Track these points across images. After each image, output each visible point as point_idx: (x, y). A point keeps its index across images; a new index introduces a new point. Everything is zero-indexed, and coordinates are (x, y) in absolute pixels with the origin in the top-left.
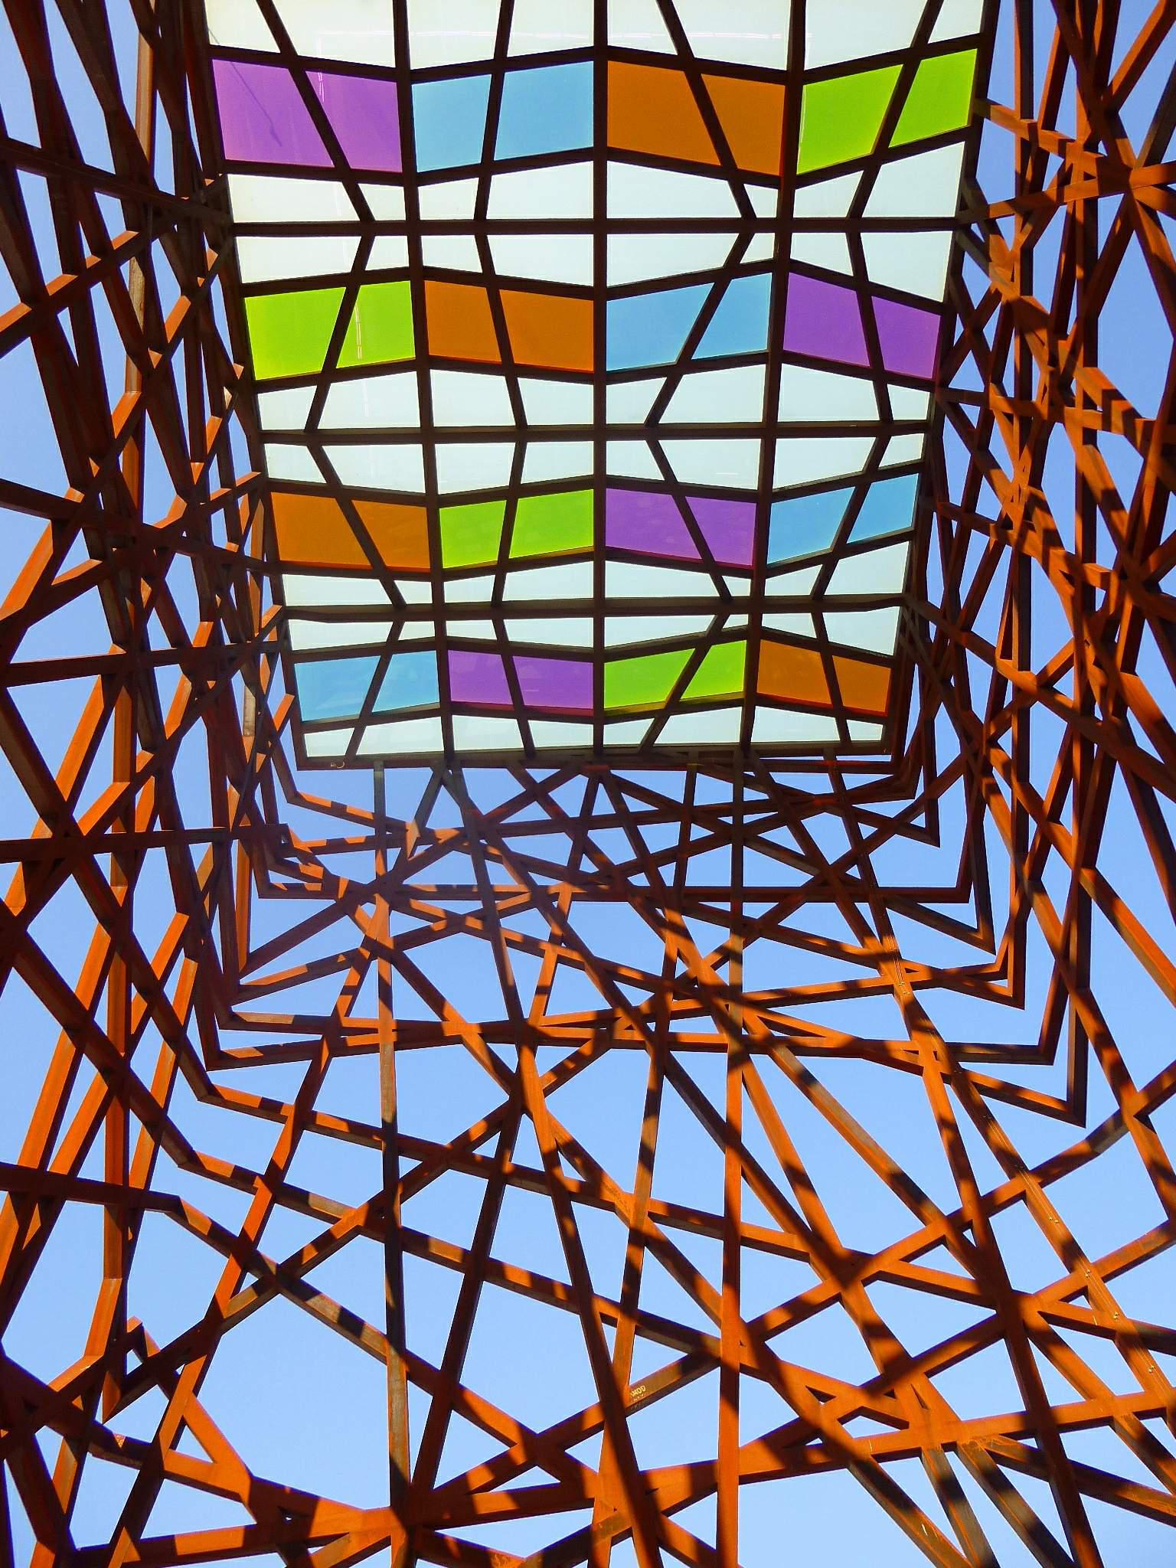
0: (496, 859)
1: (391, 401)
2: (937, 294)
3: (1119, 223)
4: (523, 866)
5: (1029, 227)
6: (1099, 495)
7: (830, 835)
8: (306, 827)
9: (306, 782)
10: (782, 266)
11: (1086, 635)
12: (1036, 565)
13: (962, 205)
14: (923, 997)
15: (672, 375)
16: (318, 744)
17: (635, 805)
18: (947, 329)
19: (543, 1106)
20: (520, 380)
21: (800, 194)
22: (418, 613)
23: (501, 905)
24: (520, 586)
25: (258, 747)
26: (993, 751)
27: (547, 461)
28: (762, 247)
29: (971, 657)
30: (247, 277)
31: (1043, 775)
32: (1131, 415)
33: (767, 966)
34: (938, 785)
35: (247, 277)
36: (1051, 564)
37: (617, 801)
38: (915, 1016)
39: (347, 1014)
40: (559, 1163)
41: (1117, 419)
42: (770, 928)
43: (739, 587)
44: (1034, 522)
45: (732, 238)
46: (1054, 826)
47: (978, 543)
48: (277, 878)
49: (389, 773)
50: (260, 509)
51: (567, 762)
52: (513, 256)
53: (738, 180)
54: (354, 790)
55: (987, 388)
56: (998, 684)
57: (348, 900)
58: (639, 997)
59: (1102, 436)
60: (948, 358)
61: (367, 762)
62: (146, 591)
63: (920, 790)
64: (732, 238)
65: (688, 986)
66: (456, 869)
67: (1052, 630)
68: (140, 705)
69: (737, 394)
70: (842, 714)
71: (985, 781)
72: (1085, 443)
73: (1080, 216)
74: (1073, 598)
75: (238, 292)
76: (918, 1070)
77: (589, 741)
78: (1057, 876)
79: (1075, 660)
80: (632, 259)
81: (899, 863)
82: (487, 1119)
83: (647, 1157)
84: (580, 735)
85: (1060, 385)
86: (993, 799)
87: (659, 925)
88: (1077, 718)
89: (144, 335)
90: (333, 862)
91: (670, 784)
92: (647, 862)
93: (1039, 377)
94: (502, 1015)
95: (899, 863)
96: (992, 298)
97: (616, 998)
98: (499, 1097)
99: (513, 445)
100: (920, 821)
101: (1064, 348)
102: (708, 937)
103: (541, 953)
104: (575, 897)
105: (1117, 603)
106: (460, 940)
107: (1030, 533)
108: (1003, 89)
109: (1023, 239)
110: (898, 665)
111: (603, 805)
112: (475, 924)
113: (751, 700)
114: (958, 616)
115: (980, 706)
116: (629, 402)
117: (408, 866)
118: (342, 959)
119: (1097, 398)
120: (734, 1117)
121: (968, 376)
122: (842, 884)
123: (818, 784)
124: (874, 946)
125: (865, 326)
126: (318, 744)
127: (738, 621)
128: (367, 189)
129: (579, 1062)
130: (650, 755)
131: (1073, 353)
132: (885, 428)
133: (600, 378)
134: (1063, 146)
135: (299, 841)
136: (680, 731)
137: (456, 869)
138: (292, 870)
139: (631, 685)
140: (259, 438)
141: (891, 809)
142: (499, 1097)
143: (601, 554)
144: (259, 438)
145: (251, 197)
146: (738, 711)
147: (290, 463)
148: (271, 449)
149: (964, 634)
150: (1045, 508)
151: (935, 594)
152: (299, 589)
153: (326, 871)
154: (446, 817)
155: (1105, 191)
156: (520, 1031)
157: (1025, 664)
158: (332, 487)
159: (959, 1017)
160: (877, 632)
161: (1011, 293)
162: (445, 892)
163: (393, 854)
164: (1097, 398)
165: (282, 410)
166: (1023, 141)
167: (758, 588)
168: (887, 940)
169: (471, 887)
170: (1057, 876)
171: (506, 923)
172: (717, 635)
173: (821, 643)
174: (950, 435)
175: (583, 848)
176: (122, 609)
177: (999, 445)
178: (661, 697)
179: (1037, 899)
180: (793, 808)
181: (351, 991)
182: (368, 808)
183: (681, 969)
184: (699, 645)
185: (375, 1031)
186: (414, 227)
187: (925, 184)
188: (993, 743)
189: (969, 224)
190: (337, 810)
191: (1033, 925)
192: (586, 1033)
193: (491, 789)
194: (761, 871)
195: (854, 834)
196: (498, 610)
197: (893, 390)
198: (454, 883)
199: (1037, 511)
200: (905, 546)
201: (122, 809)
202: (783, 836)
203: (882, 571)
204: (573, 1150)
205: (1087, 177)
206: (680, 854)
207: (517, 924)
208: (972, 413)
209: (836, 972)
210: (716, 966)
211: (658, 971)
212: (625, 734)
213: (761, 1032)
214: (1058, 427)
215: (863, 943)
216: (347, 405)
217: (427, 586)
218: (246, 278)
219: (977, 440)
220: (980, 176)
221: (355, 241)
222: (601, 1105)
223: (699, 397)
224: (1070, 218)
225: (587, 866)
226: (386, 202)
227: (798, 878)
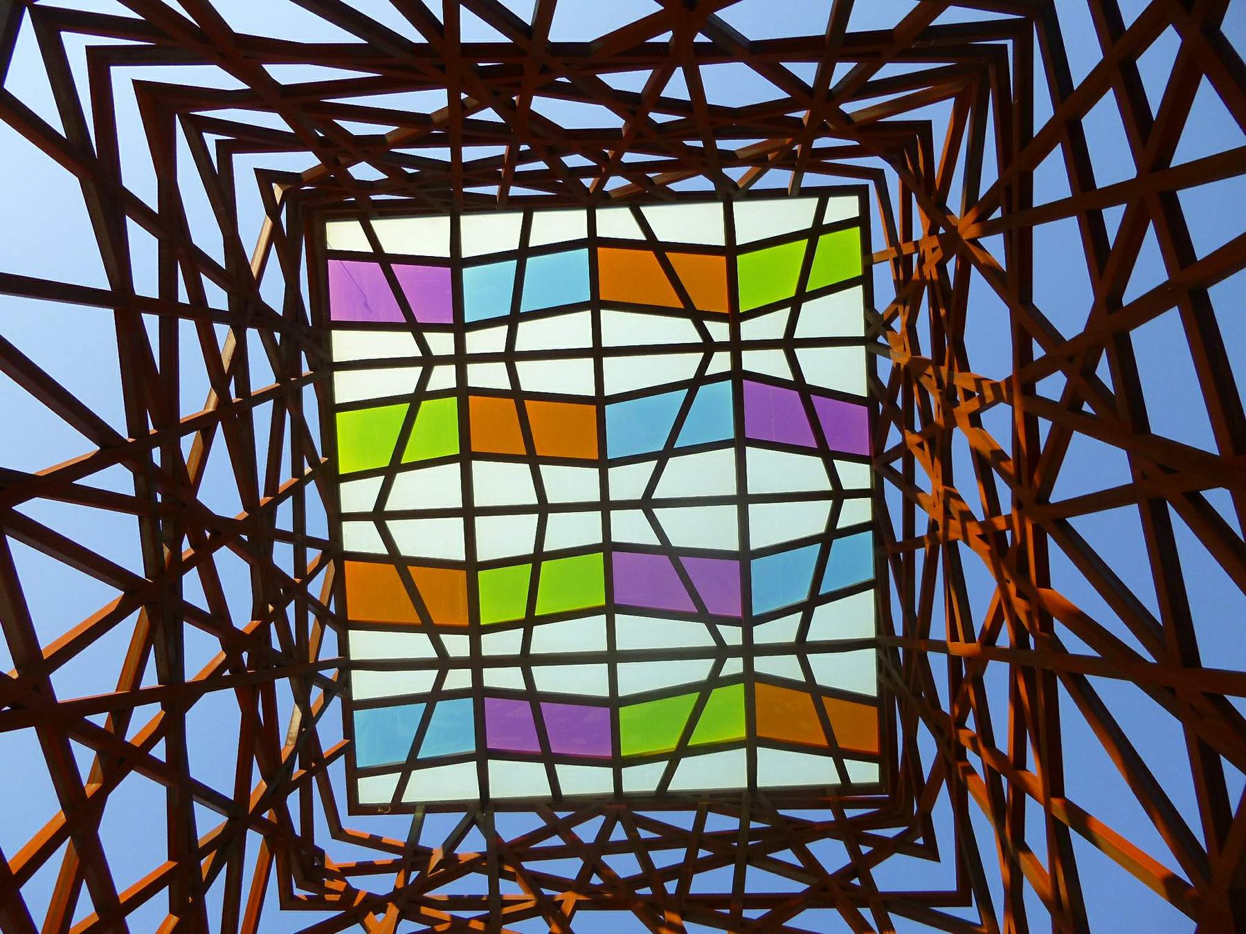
0: (511, 877)
1: (441, 486)
4: (535, 881)
5: (908, 308)
6: (989, 456)
7: (832, 855)
8: (338, 854)
10: (737, 375)
11: (1006, 575)
15: (661, 458)
17: (644, 834)
26: (961, 732)
31: (1003, 740)
32: (995, 387)
34: (928, 796)
37: (630, 830)
43: (732, 635)
45: (699, 356)
46: (1022, 773)
51: (585, 807)
52: (533, 377)
53: (699, 318)
56: (954, 663)
60: (878, 435)
61: (410, 808)
64: (699, 356)
66: (475, 884)
70: (839, 755)
71: (960, 765)
72: (972, 425)
74: (990, 552)
80: (622, 375)
81: (896, 874)
85: (949, 397)
92: (652, 876)
104: (579, 906)
107: (952, 522)
110: (882, 703)
111: (619, 833)
121: (894, 437)
123: (824, 815)
127: (734, 666)
130: (663, 798)
132: (838, 495)
133: (603, 464)
135: (331, 863)
136: (695, 775)
140: (336, 518)
145: (345, 345)
148: (347, 526)
150: (958, 497)
152: (363, 644)
153: (348, 885)
154: (474, 844)
160: (857, 674)
174: (888, 485)
177: (925, 479)
180: (799, 835)
184: (703, 690)
187: (841, 313)
188: (961, 723)
193: (511, 827)
195: (853, 851)
199: (952, 500)
201: (119, 706)
205: (934, 250)
208: (898, 465)
212: (642, 779)
217: (465, 639)
221: (418, 370)
223: (682, 476)
226: (442, 343)
227: (797, 887)
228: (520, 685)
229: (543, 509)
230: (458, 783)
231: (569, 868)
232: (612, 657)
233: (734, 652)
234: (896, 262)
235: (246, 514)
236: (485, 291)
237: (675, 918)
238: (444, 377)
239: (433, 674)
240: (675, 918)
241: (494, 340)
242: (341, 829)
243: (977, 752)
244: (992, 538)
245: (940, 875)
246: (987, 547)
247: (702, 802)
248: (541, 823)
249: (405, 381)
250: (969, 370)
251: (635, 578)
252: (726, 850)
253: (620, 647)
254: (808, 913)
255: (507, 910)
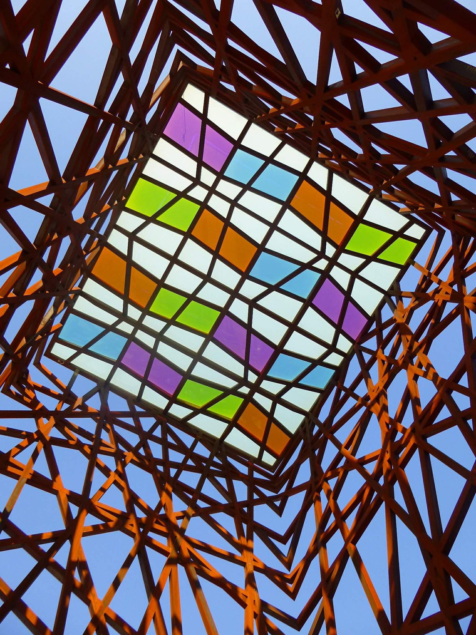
0: (107, 430)
1: (169, 241)
2: (370, 312)
3: (455, 311)
4: (118, 439)
5: (417, 302)
6: (413, 398)
7: (241, 491)
8: (35, 376)
9: (45, 361)
11: (388, 449)
12: (374, 417)
13: (392, 288)
14: (257, 575)
15: (271, 288)
16: (59, 350)
17: (170, 439)
18: (369, 325)
19: (79, 540)
20: (217, 260)
21: (343, 255)
22: (130, 321)
23: (102, 448)
24: (173, 333)
25: (41, 333)
26: (325, 483)
27: (210, 293)
28: (322, 264)
29: (329, 443)
30: (145, 172)
31: (345, 500)
32: (436, 375)
33: (197, 529)
34: (291, 491)
35: (145, 172)
36: (381, 418)
38: (250, 580)
39: (14, 456)
40: (75, 569)
41: (430, 374)
42: (205, 515)
43: (252, 378)
44: (380, 399)
47: (351, 403)
48: (13, 388)
49: (79, 377)
50: (99, 248)
51: (151, 410)
52: (239, 219)
53: (325, 239)
54: (64, 375)
55: (377, 350)
57: (38, 413)
58: (140, 514)
59: (421, 379)
60: (365, 335)
62: (55, 236)
63: (283, 490)
65: (165, 519)
66: (90, 425)
67: (373, 442)
68: (25, 275)
69: (288, 308)
71: (316, 494)
72: (414, 379)
73: (440, 304)
74: (387, 434)
75: (139, 174)
76: (244, 605)
77: (163, 407)
78: (335, 545)
79: (380, 458)
81: (263, 515)
82: (54, 533)
83: (116, 583)
84: (161, 402)
86: (317, 502)
87: (161, 489)
88: (371, 480)
89: (112, 156)
90: (40, 396)
91: (188, 440)
92: (166, 462)
93: (401, 351)
94: (80, 491)
95: (263, 515)
96: (391, 321)
97: (131, 510)
98: (61, 526)
99: (202, 280)
100: (278, 503)
101: (416, 345)
102: (178, 505)
103: (108, 475)
104: (132, 461)
105: (406, 440)
106: (77, 453)
107: (377, 404)
108: (422, 258)
109: (413, 305)
110: (294, 439)
111: (158, 433)
112: (88, 451)
113: (233, 424)
114: (329, 429)
115: (325, 465)
116: (251, 290)
117: (70, 413)
118: (24, 433)
119: (424, 365)
120: (162, 583)
121: (371, 344)
122: (241, 512)
123: (243, 469)
124: (243, 541)
125: (343, 309)
126: (59, 350)
127: (245, 390)
128: (203, 169)
129: (106, 529)
130: (183, 424)
131: (420, 347)
132: (332, 348)
133: (245, 275)
134: (440, 282)
135: (30, 380)
136: (201, 422)
137: (90, 425)
138: (22, 390)
139: (192, 394)
141: (268, 493)
142: (61, 526)
143: (209, 338)
144: (113, 225)
145: (163, 148)
146: (226, 425)
147: (118, 241)
149: (330, 434)
150: (386, 396)
151: (323, 416)
152: (91, 287)
153: (35, 396)
154: (94, 404)
155: (452, 300)
156: (84, 501)
157: (354, 453)
158: (128, 258)
159: (268, 591)
160: (292, 422)
161: (400, 320)
162: (81, 431)
163: (66, 406)
164: (424, 365)
165: (128, 221)
166: (424, 276)
167: (259, 382)
168: (250, 542)
169: (93, 435)
170: (335, 545)
171: (99, 456)
172: (234, 391)
173: (270, 416)
174: (355, 360)
175: (143, 444)
176: (45, 235)
177: (375, 372)
178: (200, 405)
179: (322, 549)
180: (231, 474)
181: (21, 448)
182: (65, 384)
183: (162, 512)
184: (227, 392)
185: (22, 470)
186: (212, 190)
187: (383, 275)
188: (326, 480)
189: (393, 294)
190: (52, 378)
191: (315, 563)
192: (114, 518)
193: (117, 404)
194: (209, 489)
195: (250, 495)
196: (160, 337)
197: (341, 336)
198: (87, 430)
199: (383, 396)
200: (318, 394)
202: (223, 481)
203: (305, 399)
204: (83, 566)
205: (447, 293)
206: (181, 467)
207: (103, 459)
209: (226, 547)
210: (178, 518)
211: (153, 508)
213: (185, 558)
214: (403, 371)
215: (239, 538)
216: (152, 233)
217: (140, 313)
218: (144, 172)
219: (366, 367)
220: (401, 283)
222: (105, 553)
223: (275, 302)
224: (435, 305)
225: (142, 451)
227: (223, 501)
228: (151, 345)
229: (207, 278)
230: (101, 370)
231: (133, 439)
232: (198, 357)
233: (248, 384)
234: (424, 278)
235: (83, 221)
236: (242, 166)
237: (170, 489)
238: (199, 193)
239: (116, 319)
240: (170, 489)
241: (232, 191)
242: (39, 364)
243: (328, 497)
244: (391, 428)
245: (280, 524)
246: (387, 430)
247: (201, 436)
248: (127, 409)
249: (181, 184)
250: (427, 354)
251: (225, 329)
252: (202, 467)
253: (204, 355)
254: (222, 514)
255: (102, 448)
